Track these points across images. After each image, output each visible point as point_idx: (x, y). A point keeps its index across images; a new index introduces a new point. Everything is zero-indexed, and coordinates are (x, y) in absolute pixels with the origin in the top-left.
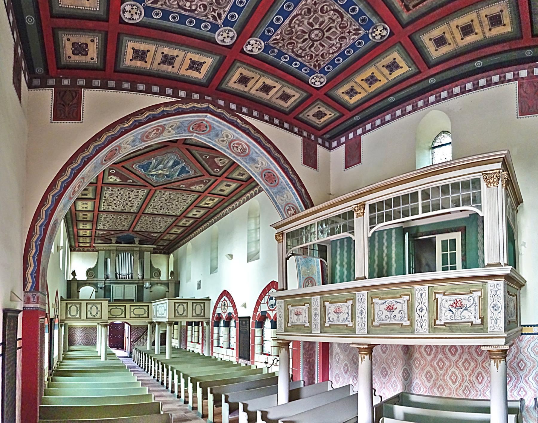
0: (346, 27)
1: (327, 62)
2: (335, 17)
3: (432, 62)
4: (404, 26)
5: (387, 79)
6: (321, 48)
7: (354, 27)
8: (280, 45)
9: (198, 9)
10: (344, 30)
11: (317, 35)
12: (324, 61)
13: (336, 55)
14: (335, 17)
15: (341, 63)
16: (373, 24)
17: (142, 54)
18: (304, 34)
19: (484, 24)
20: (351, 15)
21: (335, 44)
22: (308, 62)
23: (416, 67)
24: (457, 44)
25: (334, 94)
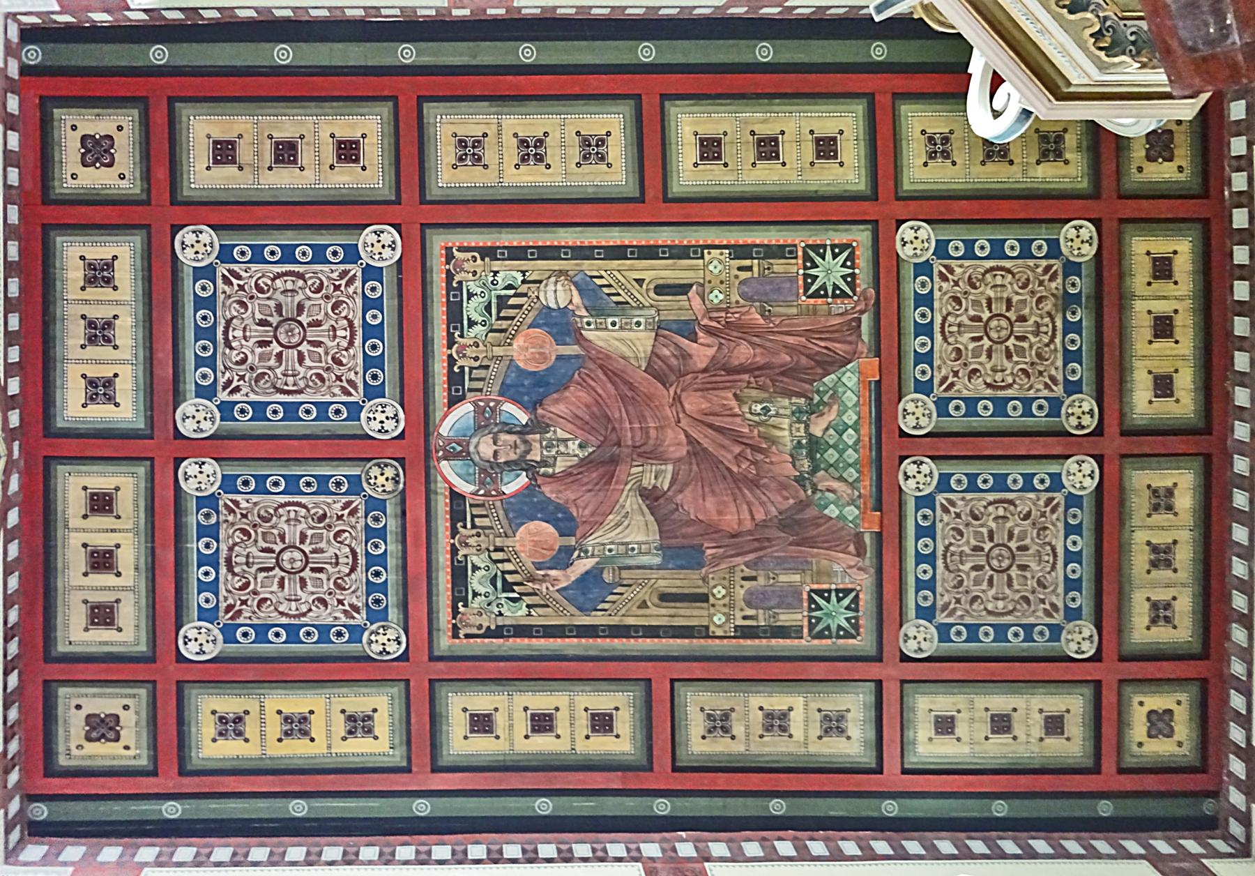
0: (344, 589)
1: (256, 621)
2: (345, 560)
3: (445, 758)
4: (433, 658)
5: (329, 747)
6: (275, 587)
7: (354, 601)
8: (230, 518)
9: (236, 352)
10: (338, 591)
11: (292, 561)
12: (254, 612)
13: (284, 620)
14: (345, 560)
15: (278, 644)
16: (386, 620)
17: (103, 277)
18: (278, 540)
19: (577, 723)
20: (367, 579)
21: (303, 601)
22: (228, 591)
23: (405, 754)
24: (512, 744)
25: (193, 700)
